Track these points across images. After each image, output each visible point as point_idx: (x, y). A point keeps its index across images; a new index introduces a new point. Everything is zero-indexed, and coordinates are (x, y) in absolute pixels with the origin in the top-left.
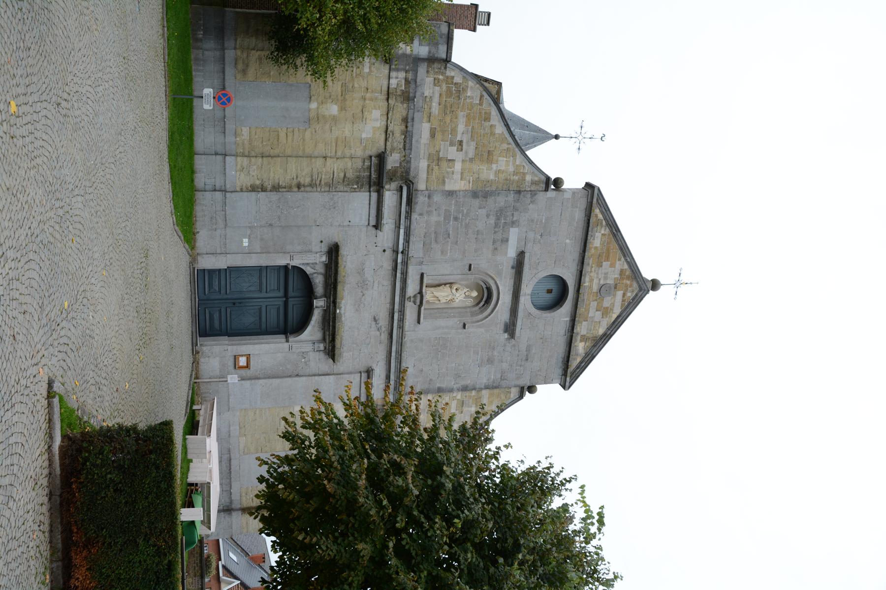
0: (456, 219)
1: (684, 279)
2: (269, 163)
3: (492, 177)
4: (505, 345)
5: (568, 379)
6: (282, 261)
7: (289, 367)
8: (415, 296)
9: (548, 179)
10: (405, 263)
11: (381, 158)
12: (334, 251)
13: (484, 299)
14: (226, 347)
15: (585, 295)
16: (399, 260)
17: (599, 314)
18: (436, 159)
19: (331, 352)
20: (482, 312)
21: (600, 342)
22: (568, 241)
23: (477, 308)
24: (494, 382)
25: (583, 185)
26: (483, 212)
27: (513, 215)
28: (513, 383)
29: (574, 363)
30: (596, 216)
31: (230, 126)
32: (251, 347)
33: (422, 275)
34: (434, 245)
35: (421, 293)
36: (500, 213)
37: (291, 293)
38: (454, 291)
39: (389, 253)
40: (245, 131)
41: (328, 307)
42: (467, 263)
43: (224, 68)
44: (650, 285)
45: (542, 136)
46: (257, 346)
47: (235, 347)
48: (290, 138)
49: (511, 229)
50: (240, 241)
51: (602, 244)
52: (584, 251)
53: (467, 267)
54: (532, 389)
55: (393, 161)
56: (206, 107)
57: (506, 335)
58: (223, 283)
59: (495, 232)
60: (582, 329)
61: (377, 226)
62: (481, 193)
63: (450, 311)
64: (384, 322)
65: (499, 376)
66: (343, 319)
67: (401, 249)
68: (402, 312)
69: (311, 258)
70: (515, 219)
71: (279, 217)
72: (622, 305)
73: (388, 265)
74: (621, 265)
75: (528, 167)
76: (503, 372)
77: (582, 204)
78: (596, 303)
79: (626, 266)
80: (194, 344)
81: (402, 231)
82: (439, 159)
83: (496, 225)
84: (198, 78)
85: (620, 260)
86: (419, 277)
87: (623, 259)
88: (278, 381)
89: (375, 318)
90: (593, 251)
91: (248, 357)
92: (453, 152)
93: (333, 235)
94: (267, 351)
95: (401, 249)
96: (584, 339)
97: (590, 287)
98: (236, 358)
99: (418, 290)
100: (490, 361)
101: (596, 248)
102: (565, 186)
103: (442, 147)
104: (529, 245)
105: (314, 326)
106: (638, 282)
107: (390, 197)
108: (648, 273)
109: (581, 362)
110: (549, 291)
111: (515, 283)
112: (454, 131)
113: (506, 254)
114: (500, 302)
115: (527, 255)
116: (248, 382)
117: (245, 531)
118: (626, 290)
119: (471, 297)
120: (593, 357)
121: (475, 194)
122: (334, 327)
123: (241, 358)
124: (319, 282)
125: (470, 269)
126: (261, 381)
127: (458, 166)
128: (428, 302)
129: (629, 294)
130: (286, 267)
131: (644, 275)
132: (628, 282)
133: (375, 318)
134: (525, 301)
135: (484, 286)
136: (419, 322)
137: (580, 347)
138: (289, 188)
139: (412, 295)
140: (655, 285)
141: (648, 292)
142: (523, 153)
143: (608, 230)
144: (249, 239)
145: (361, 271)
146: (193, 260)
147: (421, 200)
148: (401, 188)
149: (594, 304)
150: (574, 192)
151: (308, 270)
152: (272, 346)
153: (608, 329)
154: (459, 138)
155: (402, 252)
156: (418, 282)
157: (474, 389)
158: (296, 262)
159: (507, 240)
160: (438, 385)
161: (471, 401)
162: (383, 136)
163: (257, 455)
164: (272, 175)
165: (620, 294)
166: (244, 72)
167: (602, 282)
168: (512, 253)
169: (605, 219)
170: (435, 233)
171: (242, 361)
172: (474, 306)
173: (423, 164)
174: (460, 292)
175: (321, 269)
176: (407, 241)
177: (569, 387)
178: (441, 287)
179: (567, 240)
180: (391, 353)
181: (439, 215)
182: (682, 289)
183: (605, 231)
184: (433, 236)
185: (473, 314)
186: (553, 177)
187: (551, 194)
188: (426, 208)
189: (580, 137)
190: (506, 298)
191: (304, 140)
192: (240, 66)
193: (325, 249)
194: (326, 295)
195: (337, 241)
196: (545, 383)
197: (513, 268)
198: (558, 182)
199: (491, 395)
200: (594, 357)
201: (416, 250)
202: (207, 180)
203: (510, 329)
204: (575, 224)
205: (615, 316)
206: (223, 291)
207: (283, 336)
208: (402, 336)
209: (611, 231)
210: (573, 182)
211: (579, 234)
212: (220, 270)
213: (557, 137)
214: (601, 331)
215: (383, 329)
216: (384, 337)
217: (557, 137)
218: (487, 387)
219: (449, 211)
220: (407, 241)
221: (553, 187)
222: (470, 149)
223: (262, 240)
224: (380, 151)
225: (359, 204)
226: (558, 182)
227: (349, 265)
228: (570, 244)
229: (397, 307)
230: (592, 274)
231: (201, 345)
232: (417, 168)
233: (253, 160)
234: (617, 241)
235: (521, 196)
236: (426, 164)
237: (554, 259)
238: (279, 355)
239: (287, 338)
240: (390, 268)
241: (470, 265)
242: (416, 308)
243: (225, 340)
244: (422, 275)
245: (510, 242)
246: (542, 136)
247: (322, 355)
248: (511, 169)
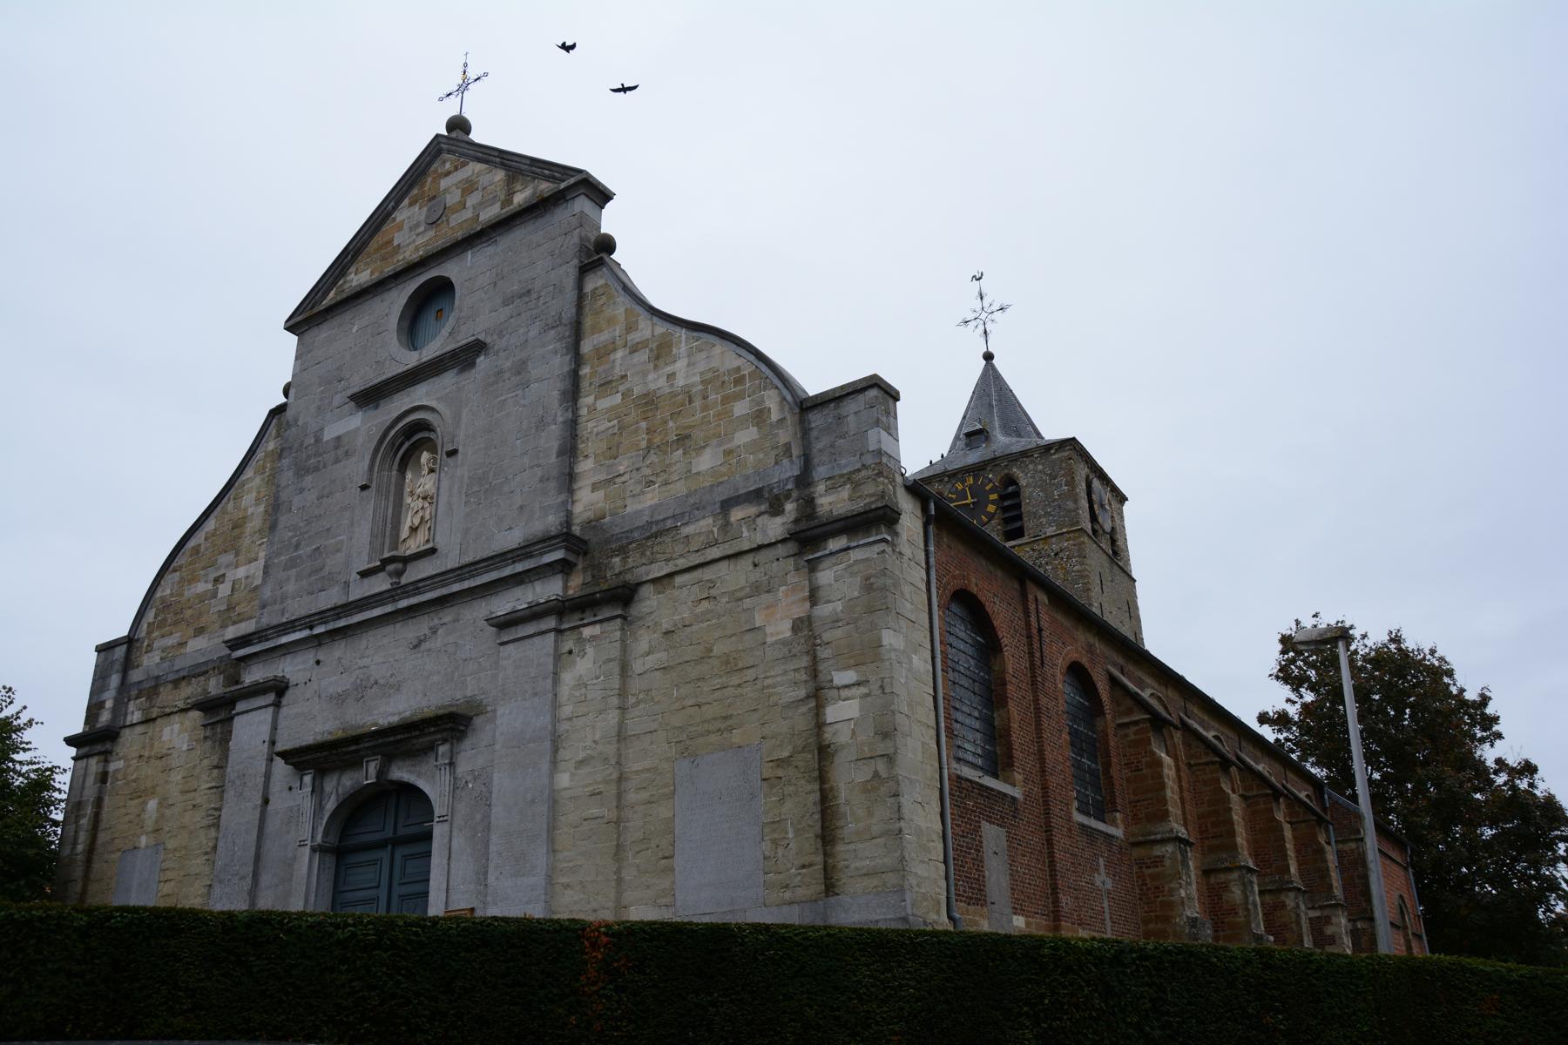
64: (420, 626)
67: (305, 633)
89: (415, 647)
95: (305, 633)
105: (419, 775)
111: (398, 391)
117: (892, 879)
133: (415, 647)
140: (458, 125)
145: (340, 699)
155: (311, 628)
176: (290, 626)
177: (580, 171)
209: (352, 262)
213: (988, 357)
216: (447, 616)
217: (988, 357)
220: (290, 626)
229: (389, 608)
234: (365, 244)
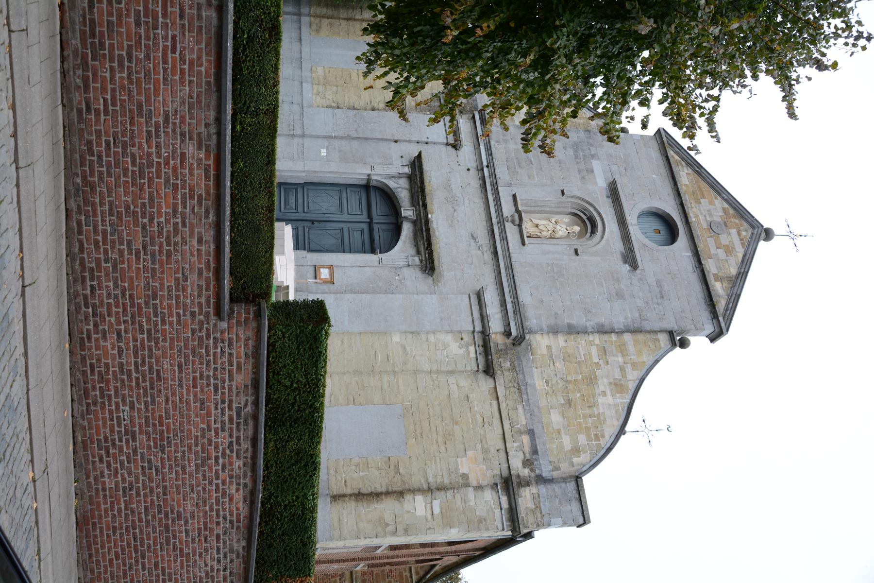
4: (630, 278)
7: (380, 284)
8: (512, 216)
12: (417, 164)
19: (429, 266)
21: (734, 299)
29: (721, 306)
31: (306, 65)
33: (514, 196)
34: (518, 170)
37: (376, 219)
39: (473, 172)
41: (418, 215)
53: (560, 193)
57: (627, 267)
58: (300, 200)
59: (577, 163)
61: (456, 146)
64: (483, 239)
65: (637, 315)
66: (437, 234)
67: (485, 163)
68: (504, 238)
69: (393, 171)
73: (475, 184)
76: (640, 311)
81: (482, 148)
86: (511, 198)
91: (331, 268)
95: (485, 163)
96: (718, 278)
97: (699, 223)
98: (316, 270)
100: (620, 295)
105: (404, 242)
109: (727, 304)
111: (616, 211)
120: (738, 296)
122: (428, 230)
123: (322, 270)
124: (403, 195)
129: (744, 234)
136: (524, 244)
137: (719, 288)
144: (327, 149)
145: (448, 187)
151: (392, 184)
155: (487, 166)
160: (567, 321)
161: (613, 347)
163: (361, 75)
166: (318, 31)
169: (683, 159)
171: (325, 273)
176: (490, 153)
180: (500, 273)
192: (314, 27)
194: (414, 203)
200: (739, 296)
206: (300, 209)
209: (695, 170)
214: (733, 271)
215: (485, 249)
216: (488, 256)
223: (340, 151)
227: (433, 179)
230: (694, 210)
244: (514, 196)
245: (596, 172)
247: (419, 274)
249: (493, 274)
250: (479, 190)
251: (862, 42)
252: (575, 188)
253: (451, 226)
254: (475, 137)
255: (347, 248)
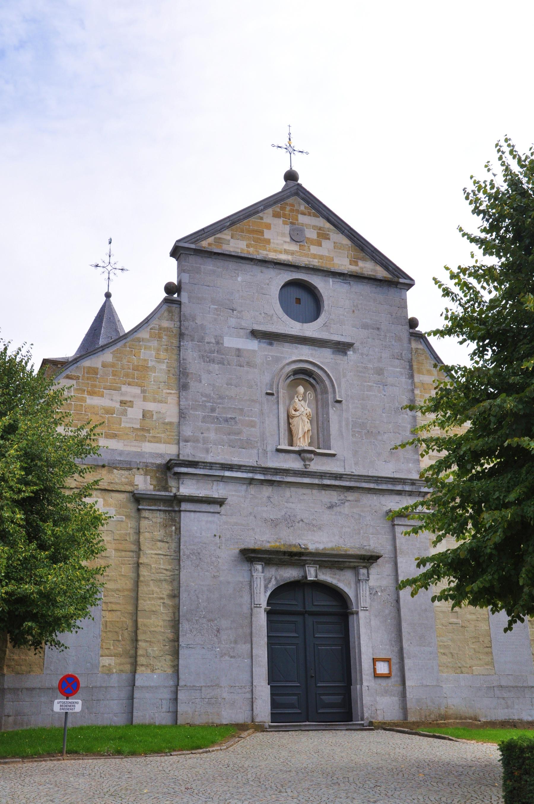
0: (213, 410)
1: (284, 142)
2: (145, 632)
3: (164, 367)
5: (402, 280)
6: (261, 619)
8: (304, 460)
9: (166, 301)
10: (265, 470)
11: (138, 499)
12: (250, 556)
13: (307, 378)
14: (364, 688)
15: (304, 261)
16: (261, 477)
17: (325, 243)
18: (142, 432)
19: (370, 559)
20: (323, 381)
22: (239, 279)
23: (317, 386)
24: (403, 368)
25: (173, 262)
26: (205, 377)
27: (208, 343)
28: (406, 345)
29: (381, 273)
30: (210, 244)
32: (364, 657)
35: (299, 453)
36: (207, 358)
38: (297, 413)
40: (106, 661)
41: (315, 562)
42: (265, 398)
43: (27, 689)
44: (292, 183)
45: (106, 316)
46: (363, 649)
47: (364, 677)
48: (114, 607)
49: (226, 345)
50: (235, 670)
51: (243, 239)
52: (251, 260)
53: (270, 397)
54: (413, 323)
55: (143, 483)
56: (78, 708)
57: (350, 353)
60: (343, 263)
61: (220, 502)
62: (182, 380)
63: (320, 419)
64: (333, 497)
67: (250, 475)
68: (322, 475)
70: (213, 341)
71: (209, 621)
72: (315, 216)
73: (267, 491)
74: (267, 216)
75: (154, 323)
76: (393, 357)
77: (193, 261)
78: (312, 247)
79: (270, 211)
80: (362, 728)
81: (227, 474)
82: (142, 429)
83: (221, 363)
84: (38, 721)
85: (262, 218)
87: (261, 214)
88: (404, 625)
90: (251, 250)
92: (134, 414)
93: (228, 553)
94: (370, 638)
97: (293, 253)
98: (377, 676)
99: (297, 456)
100: (380, 372)
101: (248, 246)
102: (175, 280)
103: (128, 425)
104: (244, 324)
106: (288, 197)
107: (187, 489)
108: (278, 185)
110: (298, 301)
112: (109, 411)
113: (254, 351)
114: (311, 360)
115: (256, 327)
116: (406, 661)
118: (298, 211)
119: (305, 393)
121: (183, 387)
123: (378, 672)
124: (290, 574)
125: (272, 394)
126: (405, 645)
127: (151, 406)
128: (310, 444)
129: (302, 208)
130: (269, 613)
131: (279, 189)
132: (288, 208)
134: (310, 330)
135: (292, 378)
136: (334, 455)
137: (367, 267)
138: (177, 608)
139: (303, 463)
141: (300, 185)
142: (126, 336)
143: (226, 232)
145: (275, 523)
146: (260, 728)
147: (189, 452)
148: (176, 474)
149: (314, 249)
150: (181, 270)
151: (273, 585)
152: (363, 630)
153: (343, 233)
154: (118, 405)
156: (287, 456)
157: (413, 391)
158: (263, 599)
159: (238, 350)
162: (114, 495)
164: (159, 629)
165: (302, 219)
167: (288, 239)
168: (253, 345)
170: (229, 435)
172: (315, 390)
173: (148, 447)
174: (298, 406)
175: (272, 572)
178: (293, 429)
179: (239, 282)
181: (208, 429)
182: (296, 144)
183: (226, 235)
184: (233, 437)
185: (325, 391)
186: (165, 295)
187: (184, 298)
188: (200, 445)
189: (108, 267)
190: (305, 353)
191: (118, 590)
193: (246, 567)
194: (302, 565)
195: (237, 551)
196: (407, 308)
197: (271, 344)
198: (170, 289)
199: (420, 372)
201: (248, 458)
202: (164, 710)
203: (342, 348)
204: (219, 270)
205: (328, 225)
207: (350, 618)
208: (351, 477)
209: (228, 227)
210: (170, 271)
211: (232, 265)
212: (272, 695)
213: (108, 295)
214: (346, 241)
216: (351, 496)
217: (108, 295)
218: (412, 377)
219: (204, 417)
220: (239, 468)
221: (176, 295)
222: (131, 391)
223: (236, 642)
224: (132, 499)
225: (195, 524)
226: (170, 289)
228: (242, 279)
229: (316, 481)
231: (362, 719)
232: (152, 455)
233: (140, 652)
235: (186, 332)
236: (147, 444)
237: (262, 299)
238: (373, 623)
239: (352, 614)
240: (270, 489)
241: (267, 394)
242: (317, 459)
243: (356, 688)
244: (279, 451)
245: (240, 346)
246: (106, 316)
248: (155, 344)
249: (369, 495)
250: (275, 488)
251: (62, 648)
252: (263, 378)
253: (320, 528)
254: (206, 478)
255: (275, 618)
